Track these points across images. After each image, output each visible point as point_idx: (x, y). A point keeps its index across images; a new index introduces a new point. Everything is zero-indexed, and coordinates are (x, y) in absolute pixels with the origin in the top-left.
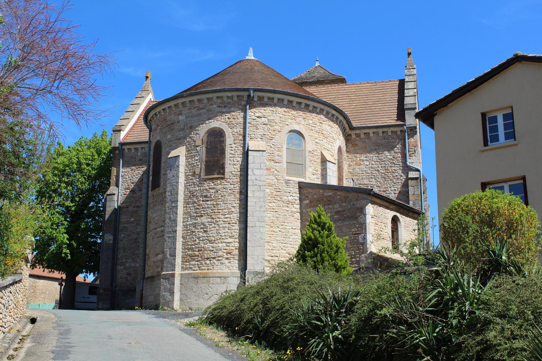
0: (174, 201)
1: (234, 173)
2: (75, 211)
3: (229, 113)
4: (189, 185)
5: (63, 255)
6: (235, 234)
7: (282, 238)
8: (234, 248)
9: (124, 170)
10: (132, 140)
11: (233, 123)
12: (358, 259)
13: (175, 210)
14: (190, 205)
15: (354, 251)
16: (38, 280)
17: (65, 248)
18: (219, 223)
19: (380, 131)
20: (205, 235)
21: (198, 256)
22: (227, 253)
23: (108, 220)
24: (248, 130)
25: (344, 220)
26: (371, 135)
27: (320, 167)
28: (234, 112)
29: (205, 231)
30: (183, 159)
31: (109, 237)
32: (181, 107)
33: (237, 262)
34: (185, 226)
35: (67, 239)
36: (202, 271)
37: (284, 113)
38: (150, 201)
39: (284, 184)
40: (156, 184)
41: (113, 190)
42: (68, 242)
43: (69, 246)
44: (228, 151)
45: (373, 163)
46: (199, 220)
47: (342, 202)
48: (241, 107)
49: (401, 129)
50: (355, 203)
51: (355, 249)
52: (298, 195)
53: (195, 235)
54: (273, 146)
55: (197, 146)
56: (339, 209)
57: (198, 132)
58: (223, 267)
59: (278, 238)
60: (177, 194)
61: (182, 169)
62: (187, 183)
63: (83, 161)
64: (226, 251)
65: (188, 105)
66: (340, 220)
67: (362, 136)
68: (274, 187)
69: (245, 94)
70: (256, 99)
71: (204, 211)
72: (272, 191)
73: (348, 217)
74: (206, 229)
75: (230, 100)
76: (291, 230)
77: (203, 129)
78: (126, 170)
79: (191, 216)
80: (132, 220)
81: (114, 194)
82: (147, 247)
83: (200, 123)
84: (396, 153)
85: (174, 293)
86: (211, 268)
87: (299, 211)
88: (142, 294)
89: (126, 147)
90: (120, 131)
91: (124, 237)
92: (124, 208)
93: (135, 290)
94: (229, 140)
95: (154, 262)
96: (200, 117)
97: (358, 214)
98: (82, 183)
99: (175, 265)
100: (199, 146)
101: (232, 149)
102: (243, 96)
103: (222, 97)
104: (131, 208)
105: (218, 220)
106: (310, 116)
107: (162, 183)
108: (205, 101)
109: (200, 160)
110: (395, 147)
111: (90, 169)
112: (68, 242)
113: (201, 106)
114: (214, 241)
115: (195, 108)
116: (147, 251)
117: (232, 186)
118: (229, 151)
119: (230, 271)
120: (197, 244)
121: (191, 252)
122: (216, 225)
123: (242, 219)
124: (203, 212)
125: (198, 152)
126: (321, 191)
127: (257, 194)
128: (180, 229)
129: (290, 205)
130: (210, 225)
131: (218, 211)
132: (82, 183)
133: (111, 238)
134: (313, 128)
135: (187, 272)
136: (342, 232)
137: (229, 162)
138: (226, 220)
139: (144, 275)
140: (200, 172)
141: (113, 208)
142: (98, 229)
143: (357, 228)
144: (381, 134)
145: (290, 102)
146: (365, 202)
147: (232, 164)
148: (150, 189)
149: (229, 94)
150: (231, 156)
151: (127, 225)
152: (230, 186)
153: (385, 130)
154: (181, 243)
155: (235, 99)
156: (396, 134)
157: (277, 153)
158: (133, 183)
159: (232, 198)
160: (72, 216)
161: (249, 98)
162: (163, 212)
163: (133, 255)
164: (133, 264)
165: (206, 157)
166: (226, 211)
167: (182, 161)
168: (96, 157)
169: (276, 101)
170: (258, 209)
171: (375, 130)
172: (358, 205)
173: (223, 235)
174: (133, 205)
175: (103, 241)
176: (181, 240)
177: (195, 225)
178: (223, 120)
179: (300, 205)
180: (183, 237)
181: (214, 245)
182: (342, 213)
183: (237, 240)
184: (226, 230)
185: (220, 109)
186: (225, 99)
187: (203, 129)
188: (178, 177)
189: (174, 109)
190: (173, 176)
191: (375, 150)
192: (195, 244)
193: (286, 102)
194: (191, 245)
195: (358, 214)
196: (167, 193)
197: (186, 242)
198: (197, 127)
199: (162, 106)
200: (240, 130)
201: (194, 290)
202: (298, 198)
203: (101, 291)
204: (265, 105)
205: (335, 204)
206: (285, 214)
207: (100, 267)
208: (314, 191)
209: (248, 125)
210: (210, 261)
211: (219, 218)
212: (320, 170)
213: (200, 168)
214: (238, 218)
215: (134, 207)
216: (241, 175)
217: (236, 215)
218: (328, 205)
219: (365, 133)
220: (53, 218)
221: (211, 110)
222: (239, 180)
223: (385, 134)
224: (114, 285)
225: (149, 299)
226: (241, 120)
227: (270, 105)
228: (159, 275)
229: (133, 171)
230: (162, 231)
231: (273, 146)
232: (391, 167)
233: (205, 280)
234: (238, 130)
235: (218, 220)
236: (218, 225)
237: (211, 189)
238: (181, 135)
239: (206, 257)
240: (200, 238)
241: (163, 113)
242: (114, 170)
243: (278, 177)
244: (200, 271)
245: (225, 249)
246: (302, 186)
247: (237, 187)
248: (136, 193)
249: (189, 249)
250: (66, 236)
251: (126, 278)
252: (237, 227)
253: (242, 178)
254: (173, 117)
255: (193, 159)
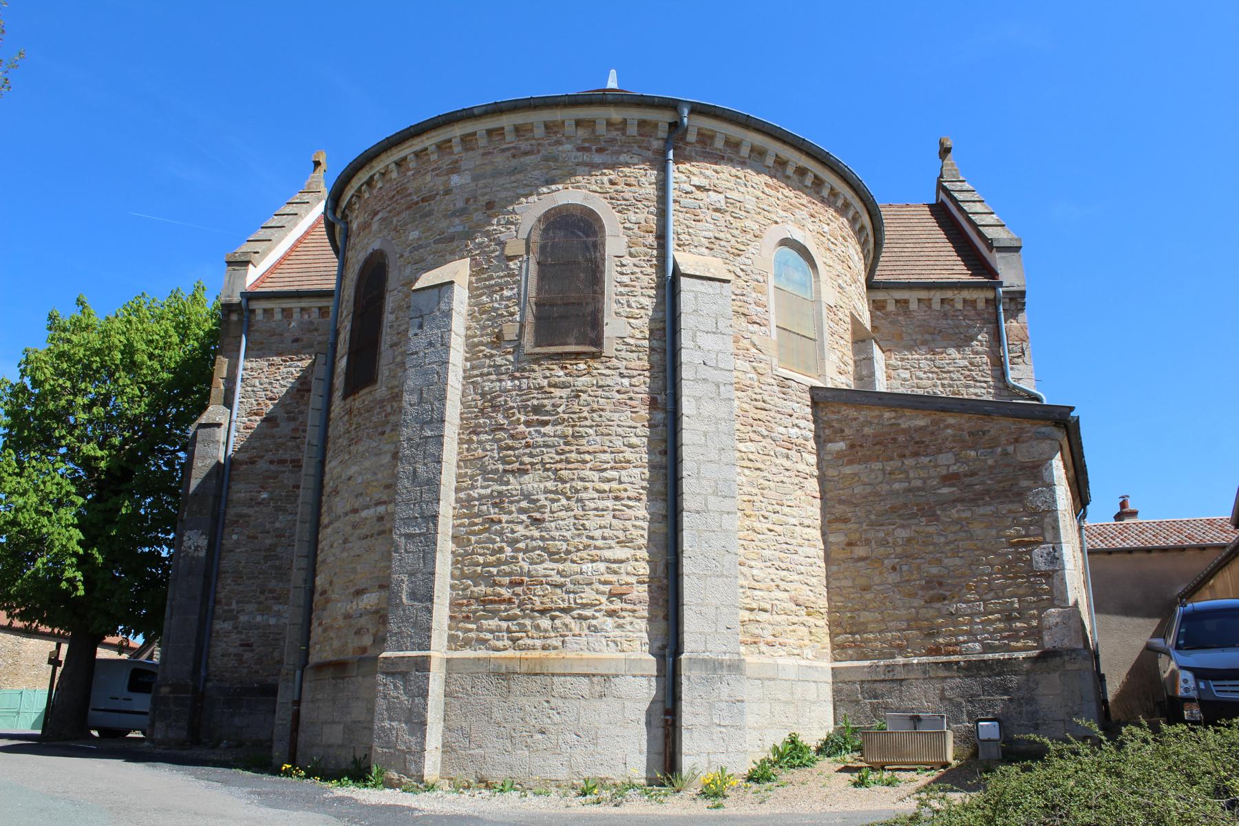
0: (431, 421)
1: (632, 341)
2: (108, 471)
3: (613, 167)
4: (482, 375)
5: (64, 585)
6: (635, 533)
7: (777, 553)
8: (633, 580)
9: (249, 365)
10: (277, 288)
11: (626, 195)
12: (1034, 623)
13: (431, 449)
14: (484, 437)
15: (1019, 598)
16: (25, 640)
17: (71, 565)
18: (584, 495)
19: (937, 296)
20: (536, 534)
21: (510, 601)
22: (611, 595)
23: (195, 493)
24: (671, 219)
25: (976, 499)
26: (913, 306)
27: (850, 354)
28: (627, 165)
29: (536, 521)
30: (463, 300)
31: (195, 541)
32: (457, 149)
33: (643, 625)
34: (465, 503)
35: (80, 543)
36: (523, 654)
37: (766, 190)
38: (337, 428)
39: (776, 388)
40: (363, 370)
41: (217, 414)
42: (81, 551)
43: (84, 562)
44: (611, 273)
45: (921, 374)
46: (514, 484)
47: (963, 448)
48: (649, 154)
49: (990, 295)
50: (1010, 449)
51: (1021, 591)
52: (812, 427)
53: (500, 533)
54: (741, 274)
55: (510, 258)
56: (953, 469)
57: (512, 218)
58: (597, 641)
59: (766, 553)
60: (442, 398)
61: (459, 324)
62: (473, 368)
63: (141, 346)
64: (606, 588)
65: (483, 142)
66: (962, 501)
67: (891, 307)
68: (750, 393)
69: (664, 117)
70: (692, 137)
71: (531, 455)
72: (746, 406)
73: (987, 492)
74: (537, 515)
75: (614, 134)
76: (798, 529)
77: (531, 211)
78: (254, 365)
79: (484, 471)
80: (264, 495)
81: (219, 425)
82: (319, 568)
83: (521, 191)
84: (977, 353)
85: (424, 723)
86: (556, 642)
87: (816, 473)
88: (296, 716)
89: (259, 306)
90: (246, 263)
91: (237, 542)
92: (242, 463)
93: (270, 691)
94: (614, 244)
95: (347, 616)
96: (519, 176)
97: (1024, 483)
98: (131, 400)
99: (429, 629)
100: (516, 257)
101: (624, 270)
102: (656, 126)
103: (592, 123)
104: (262, 465)
105: (580, 485)
106: (822, 211)
107: (384, 371)
108: (539, 132)
109: (519, 300)
110: (973, 338)
111: (157, 366)
112: (81, 551)
113: (524, 146)
114: (568, 552)
115: (503, 151)
116: (318, 581)
117: (626, 381)
118: (615, 274)
119: (622, 655)
120: (506, 563)
121: (482, 589)
122: (572, 503)
123: (659, 487)
124: (526, 459)
125: (514, 275)
126: (887, 415)
127: (708, 408)
128: (447, 508)
129: (792, 453)
130: (553, 501)
131: (579, 457)
132: (132, 399)
133: (203, 542)
134: (833, 247)
135: (468, 653)
136: (971, 538)
137: (615, 307)
138: (606, 487)
139: (307, 653)
140: (520, 335)
141: (214, 462)
142: (167, 521)
143: (1026, 526)
144: (936, 305)
145: (781, 163)
146: (1045, 446)
147: (626, 316)
148: (339, 382)
149: (616, 114)
150: (622, 289)
151: (250, 511)
152: (619, 380)
153: (949, 294)
154: (449, 558)
155: (633, 130)
156: (975, 308)
157: (754, 295)
158: (271, 399)
159: (625, 417)
160: (101, 486)
161: (671, 130)
162: (386, 459)
163: (262, 592)
164: (259, 618)
165: (539, 289)
166: (607, 457)
167: (460, 299)
168: (175, 339)
169: (745, 151)
170: (713, 455)
171: (923, 294)
172: (1023, 454)
173: (598, 534)
174: (270, 456)
175: (178, 551)
176: (450, 546)
177: (499, 501)
178: (594, 187)
179: (818, 455)
180: (454, 537)
181: (568, 566)
182: (967, 480)
183: (644, 554)
184: (608, 518)
185: (586, 157)
186: (601, 129)
187: (531, 211)
188: (446, 346)
189: (434, 157)
190: (431, 344)
191: (924, 343)
192: (499, 563)
193: (770, 161)
194: (485, 565)
195: (1024, 483)
196: (406, 397)
197: (467, 554)
198: (512, 203)
199: (394, 150)
200: (645, 216)
201: (497, 715)
202: (811, 435)
203: (165, 690)
204: (717, 158)
205: (940, 451)
206: (781, 478)
207: (166, 624)
208: (864, 415)
209: (672, 207)
210: (553, 618)
211: (582, 479)
212: (851, 362)
213: (518, 320)
214: (645, 484)
215: (272, 462)
216: (652, 349)
217: (637, 471)
218: (916, 454)
219: (897, 301)
220: (44, 483)
221: (555, 159)
222: (647, 365)
223: (947, 307)
224: (203, 673)
225: (326, 729)
226: (651, 191)
227: (730, 161)
228: (366, 662)
229: (273, 369)
230: (380, 519)
231: (741, 274)
232: (968, 387)
233: (536, 684)
234: (641, 217)
235: (580, 485)
236: (579, 500)
237: (555, 386)
238: (457, 226)
239: (538, 606)
240: (517, 541)
241: (394, 175)
242: (222, 366)
243: (761, 367)
244: (518, 654)
245: (605, 583)
246: (821, 399)
247: (642, 385)
248: (277, 426)
249: (476, 578)
250: (77, 534)
251: (239, 657)
252: (641, 511)
253: (656, 357)
254: (429, 181)
255: (496, 296)
